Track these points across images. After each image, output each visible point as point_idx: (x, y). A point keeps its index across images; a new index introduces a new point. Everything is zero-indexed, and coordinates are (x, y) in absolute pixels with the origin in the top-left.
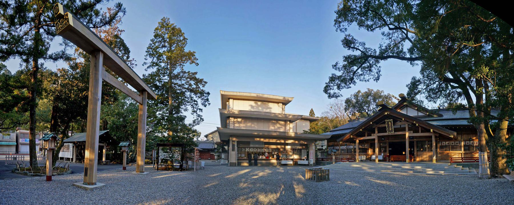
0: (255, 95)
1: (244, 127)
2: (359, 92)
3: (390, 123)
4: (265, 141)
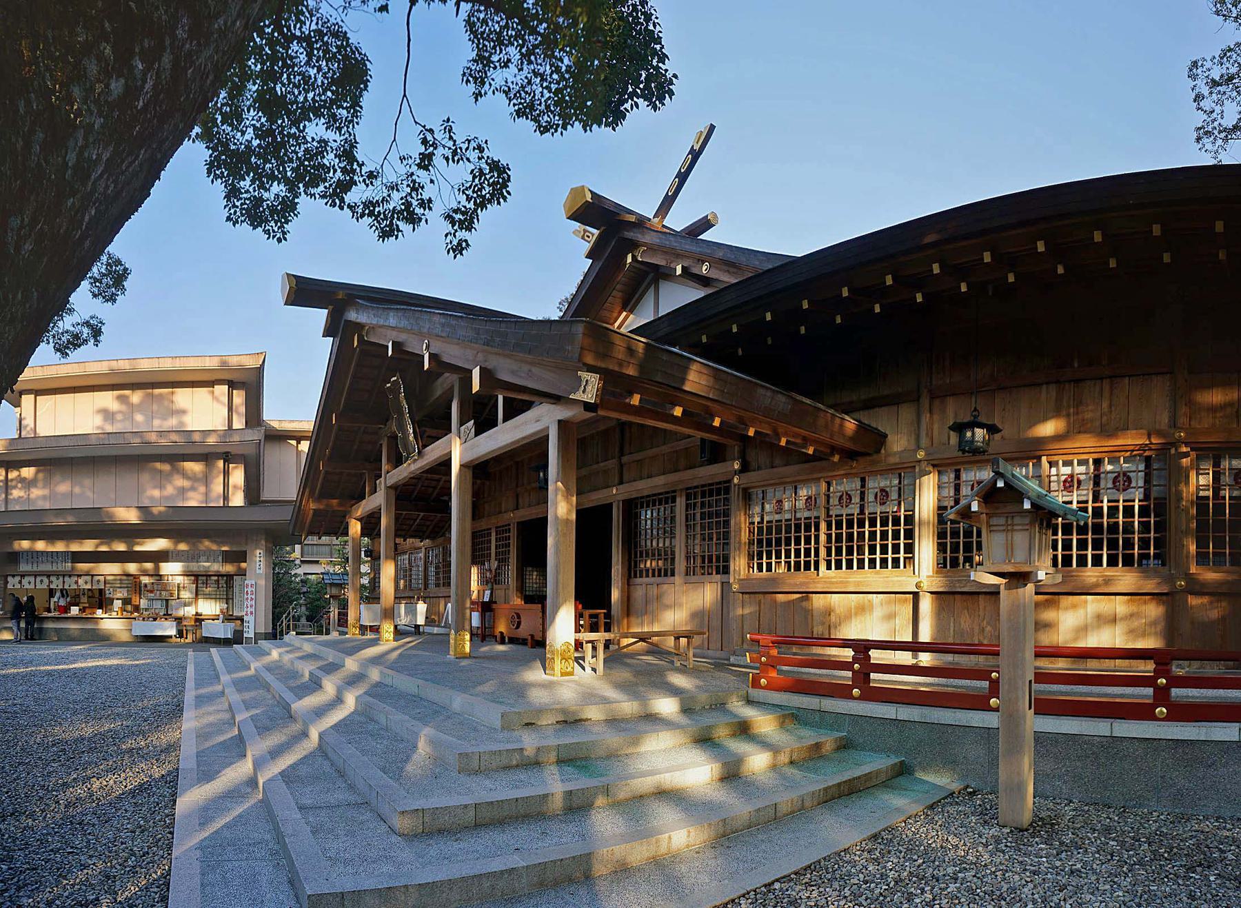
0: (103, 368)
1: (44, 498)
4: (50, 549)
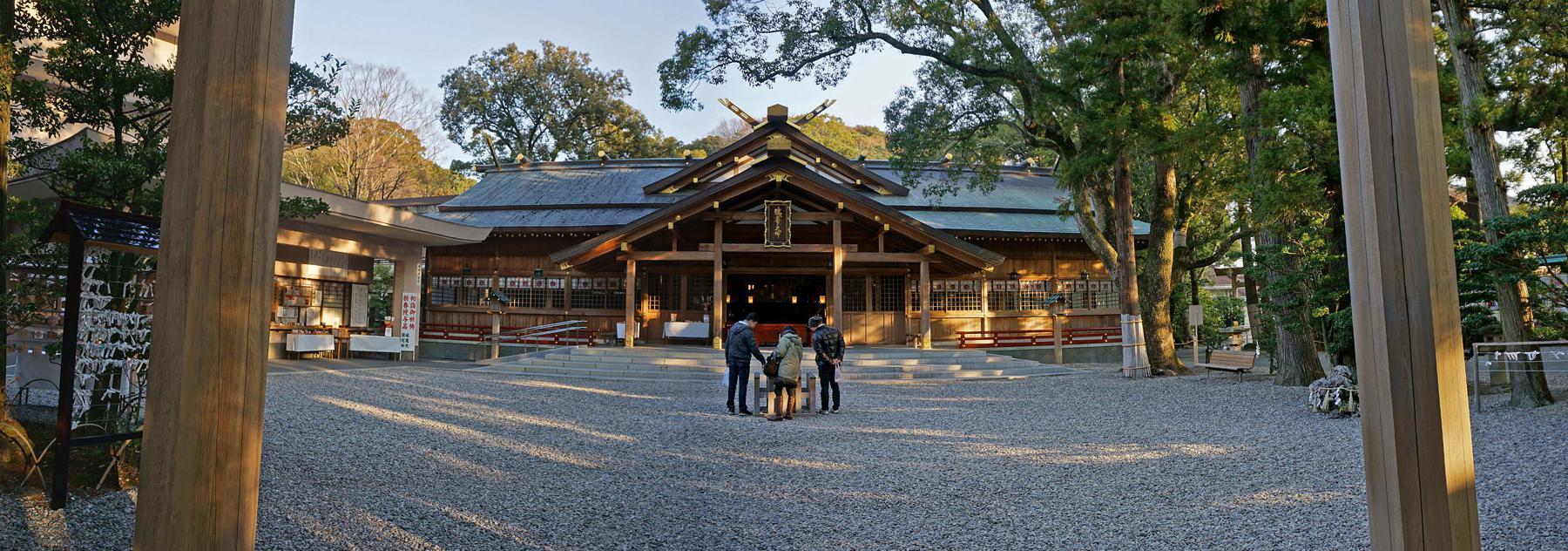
2: (511, 49)
3: (777, 211)
